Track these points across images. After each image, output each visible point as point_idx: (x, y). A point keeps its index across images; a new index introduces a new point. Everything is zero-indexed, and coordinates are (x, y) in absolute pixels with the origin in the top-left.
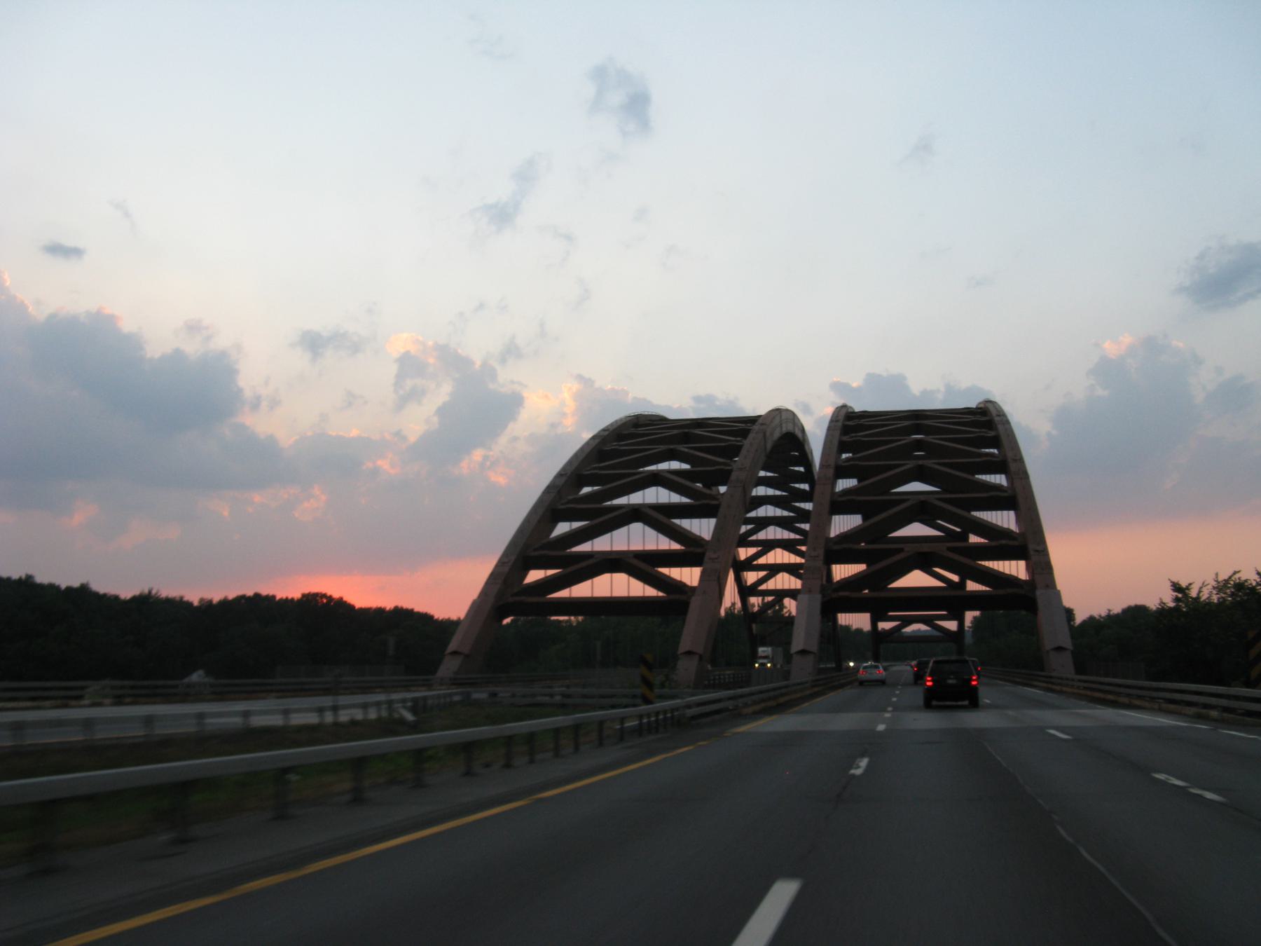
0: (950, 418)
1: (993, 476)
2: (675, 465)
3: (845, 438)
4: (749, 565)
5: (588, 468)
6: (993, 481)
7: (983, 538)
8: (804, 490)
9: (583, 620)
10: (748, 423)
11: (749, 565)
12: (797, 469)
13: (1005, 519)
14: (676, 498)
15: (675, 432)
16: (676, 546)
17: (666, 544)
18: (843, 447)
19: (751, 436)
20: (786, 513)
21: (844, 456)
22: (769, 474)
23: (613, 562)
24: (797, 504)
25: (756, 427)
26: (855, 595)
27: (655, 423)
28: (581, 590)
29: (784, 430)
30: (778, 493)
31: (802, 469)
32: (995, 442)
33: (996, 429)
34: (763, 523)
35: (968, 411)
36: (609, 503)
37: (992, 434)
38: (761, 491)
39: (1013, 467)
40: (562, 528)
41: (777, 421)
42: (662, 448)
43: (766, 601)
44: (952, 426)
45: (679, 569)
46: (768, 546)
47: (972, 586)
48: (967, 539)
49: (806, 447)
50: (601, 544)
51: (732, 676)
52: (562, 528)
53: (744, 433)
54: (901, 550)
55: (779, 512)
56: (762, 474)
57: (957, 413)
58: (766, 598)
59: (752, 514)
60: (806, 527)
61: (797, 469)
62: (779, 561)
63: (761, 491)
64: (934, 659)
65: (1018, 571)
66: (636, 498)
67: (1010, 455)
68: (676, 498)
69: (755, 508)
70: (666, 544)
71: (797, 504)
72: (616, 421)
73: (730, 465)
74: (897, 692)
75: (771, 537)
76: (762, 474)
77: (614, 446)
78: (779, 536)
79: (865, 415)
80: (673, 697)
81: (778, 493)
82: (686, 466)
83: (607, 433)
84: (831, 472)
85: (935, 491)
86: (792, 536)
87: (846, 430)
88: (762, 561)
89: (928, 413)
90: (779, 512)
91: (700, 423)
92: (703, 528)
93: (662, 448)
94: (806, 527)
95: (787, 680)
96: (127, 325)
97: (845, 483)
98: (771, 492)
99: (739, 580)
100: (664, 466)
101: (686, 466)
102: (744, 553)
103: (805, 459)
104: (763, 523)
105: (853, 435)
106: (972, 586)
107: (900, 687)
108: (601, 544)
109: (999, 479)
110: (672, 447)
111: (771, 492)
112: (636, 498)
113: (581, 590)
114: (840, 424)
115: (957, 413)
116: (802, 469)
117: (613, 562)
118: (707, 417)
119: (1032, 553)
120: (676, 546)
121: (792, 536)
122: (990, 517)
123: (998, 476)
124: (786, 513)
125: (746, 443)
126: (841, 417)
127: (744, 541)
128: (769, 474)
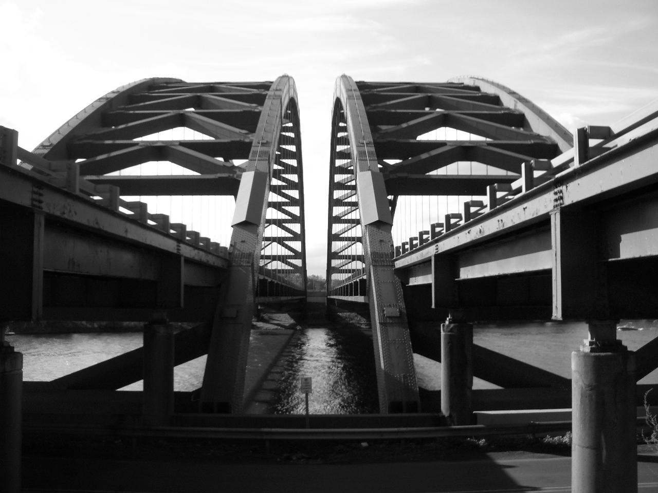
9: (545, 437)
10: (261, 89)
15: (188, 95)
16: (290, 218)
19: (268, 102)
25: (270, 93)
27: (169, 85)
42: (172, 112)
53: (260, 100)
60: (276, 167)
64: (418, 247)
65: (194, 135)
72: (140, 80)
85: (287, 132)
89: (427, 86)
91: (212, 87)
93: (172, 112)
94: (276, 167)
105: (374, 105)
118: (651, 121)
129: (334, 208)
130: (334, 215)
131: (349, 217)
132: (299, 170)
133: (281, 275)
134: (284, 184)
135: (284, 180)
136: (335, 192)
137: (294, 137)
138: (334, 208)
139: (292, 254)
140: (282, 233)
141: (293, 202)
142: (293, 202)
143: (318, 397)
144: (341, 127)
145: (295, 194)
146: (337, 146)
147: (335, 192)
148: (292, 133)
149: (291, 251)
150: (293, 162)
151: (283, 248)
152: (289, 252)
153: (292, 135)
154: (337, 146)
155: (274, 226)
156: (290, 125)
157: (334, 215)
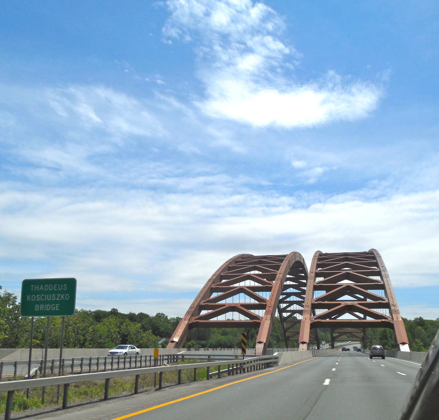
0: (358, 255)
1: (373, 277)
2: (257, 272)
3: (319, 263)
4: (284, 310)
5: (225, 273)
6: (375, 278)
7: (211, 310)
13: (379, 293)
14: (257, 284)
17: (253, 301)
18: (318, 266)
20: (297, 291)
21: (319, 269)
22: (291, 277)
23: (233, 308)
26: (323, 321)
28: (221, 318)
29: (297, 260)
30: (294, 283)
31: (303, 275)
32: (376, 264)
33: (376, 259)
34: (289, 295)
35: (365, 253)
36: (232, 286)
37: (375, 261)
38: (288, 283)
39: (383, 273)
40: (215, 295)
42: (252, 266)
44: (269, 261)
46: (292, 303)
47: (369, 319)
48: (366, 301)
49: (305, 266)
50: (229, 301)
51: (48, 371)
52: (215, 295)
54: (340, 304)
55: (295, 291)
56: (288, 276)
57: (279, 257)
59: (285, 292)
63: (288, 283)
66: (242, 284)
67: (382, 269)
68: (257, 284)
69: (286, 290)
70: (253, 301)
73: (277, 272)
74: (340, 358)
75: (292, 300)
76: (288, 276)
77: (234, 265)
78: (295, 300)
79: (326, 254)
80: (214, 362)
81: (294, 283)
82: (260, 273)
83: (231, 260)
84: (313, 275)
87: (319, 260)
88: (288, 309)
90: (295, 291)
92: (266, 295)
93: (252, 266)
95: (343, 348)
97: (322, 278)
98: (292, 283)
100: (253, 272)
101: (260, 273)
102: (283, 306)
103: (304, 270)
104: (289, 295)
106: (369, 319)
107: (341, 357)
108: (229, 301)
109: (378, 278)
110: (255, 265)
111: (292, 283)
112: (242, 284)
113: (221, 318)
114: (317, 258)
115: (279, 257)
116: (303, 275)
117: (233, 308)
119: (391, 306)
120: (257, 302)
122: (374, 292)
123: (377, 277)
124: (297, 291)
125: (282, 264)
126: (318, 255)
127: (282, 301)
128: (291, 277)
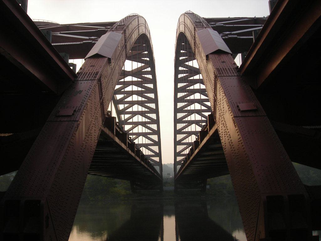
4: (122, 101)
8: (150, 88)
11: (122, 101)
12: (145, 59)
20: (140, 89)
24: (146, 85)
31: (148, 59)
41: (135, 23)
43: (125, 106)
45: (81, 59)
58: (125, 105)
61: (145, 59)
62: (140, 131)
71: (146, 85)
78: (140, 120)
86: (144, 109)
96: (73, 231)
99: (117, 108)
102: (119, 97)
116: (148, 59)
121: (144, 109)
124: (140, 89)
129: (178, 114)
130: (177, 129)
131: (186, 130)
132: (155, 91)
133: (128, 85)
134: (149, 125)
135: (146, 97)
136: (178, 114)
137: (151, 78)
138: (178, 114)
139: (153, 154)
140: (145, 130)
141: (152, 111)
142: (152, 111)
143: (74, 109)
144: (182, 53)
145: (153, 106)
146: (179, 84)
147: (178, 114)
148: (150, 75)
149: (152, 152)
150: (151, 86)
151: (147, 140)
152: (149, 141)
153: (150, 77)
154: (179, 84)
155: (140, 127)
156: (149, 69)
157: (177, 129)
